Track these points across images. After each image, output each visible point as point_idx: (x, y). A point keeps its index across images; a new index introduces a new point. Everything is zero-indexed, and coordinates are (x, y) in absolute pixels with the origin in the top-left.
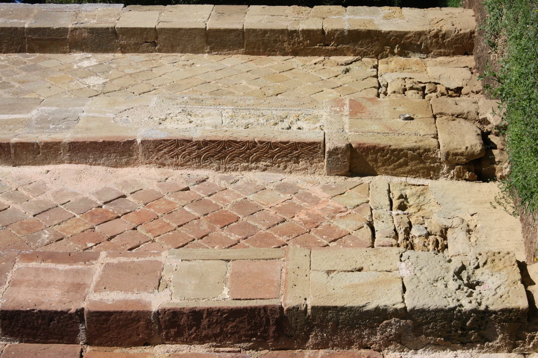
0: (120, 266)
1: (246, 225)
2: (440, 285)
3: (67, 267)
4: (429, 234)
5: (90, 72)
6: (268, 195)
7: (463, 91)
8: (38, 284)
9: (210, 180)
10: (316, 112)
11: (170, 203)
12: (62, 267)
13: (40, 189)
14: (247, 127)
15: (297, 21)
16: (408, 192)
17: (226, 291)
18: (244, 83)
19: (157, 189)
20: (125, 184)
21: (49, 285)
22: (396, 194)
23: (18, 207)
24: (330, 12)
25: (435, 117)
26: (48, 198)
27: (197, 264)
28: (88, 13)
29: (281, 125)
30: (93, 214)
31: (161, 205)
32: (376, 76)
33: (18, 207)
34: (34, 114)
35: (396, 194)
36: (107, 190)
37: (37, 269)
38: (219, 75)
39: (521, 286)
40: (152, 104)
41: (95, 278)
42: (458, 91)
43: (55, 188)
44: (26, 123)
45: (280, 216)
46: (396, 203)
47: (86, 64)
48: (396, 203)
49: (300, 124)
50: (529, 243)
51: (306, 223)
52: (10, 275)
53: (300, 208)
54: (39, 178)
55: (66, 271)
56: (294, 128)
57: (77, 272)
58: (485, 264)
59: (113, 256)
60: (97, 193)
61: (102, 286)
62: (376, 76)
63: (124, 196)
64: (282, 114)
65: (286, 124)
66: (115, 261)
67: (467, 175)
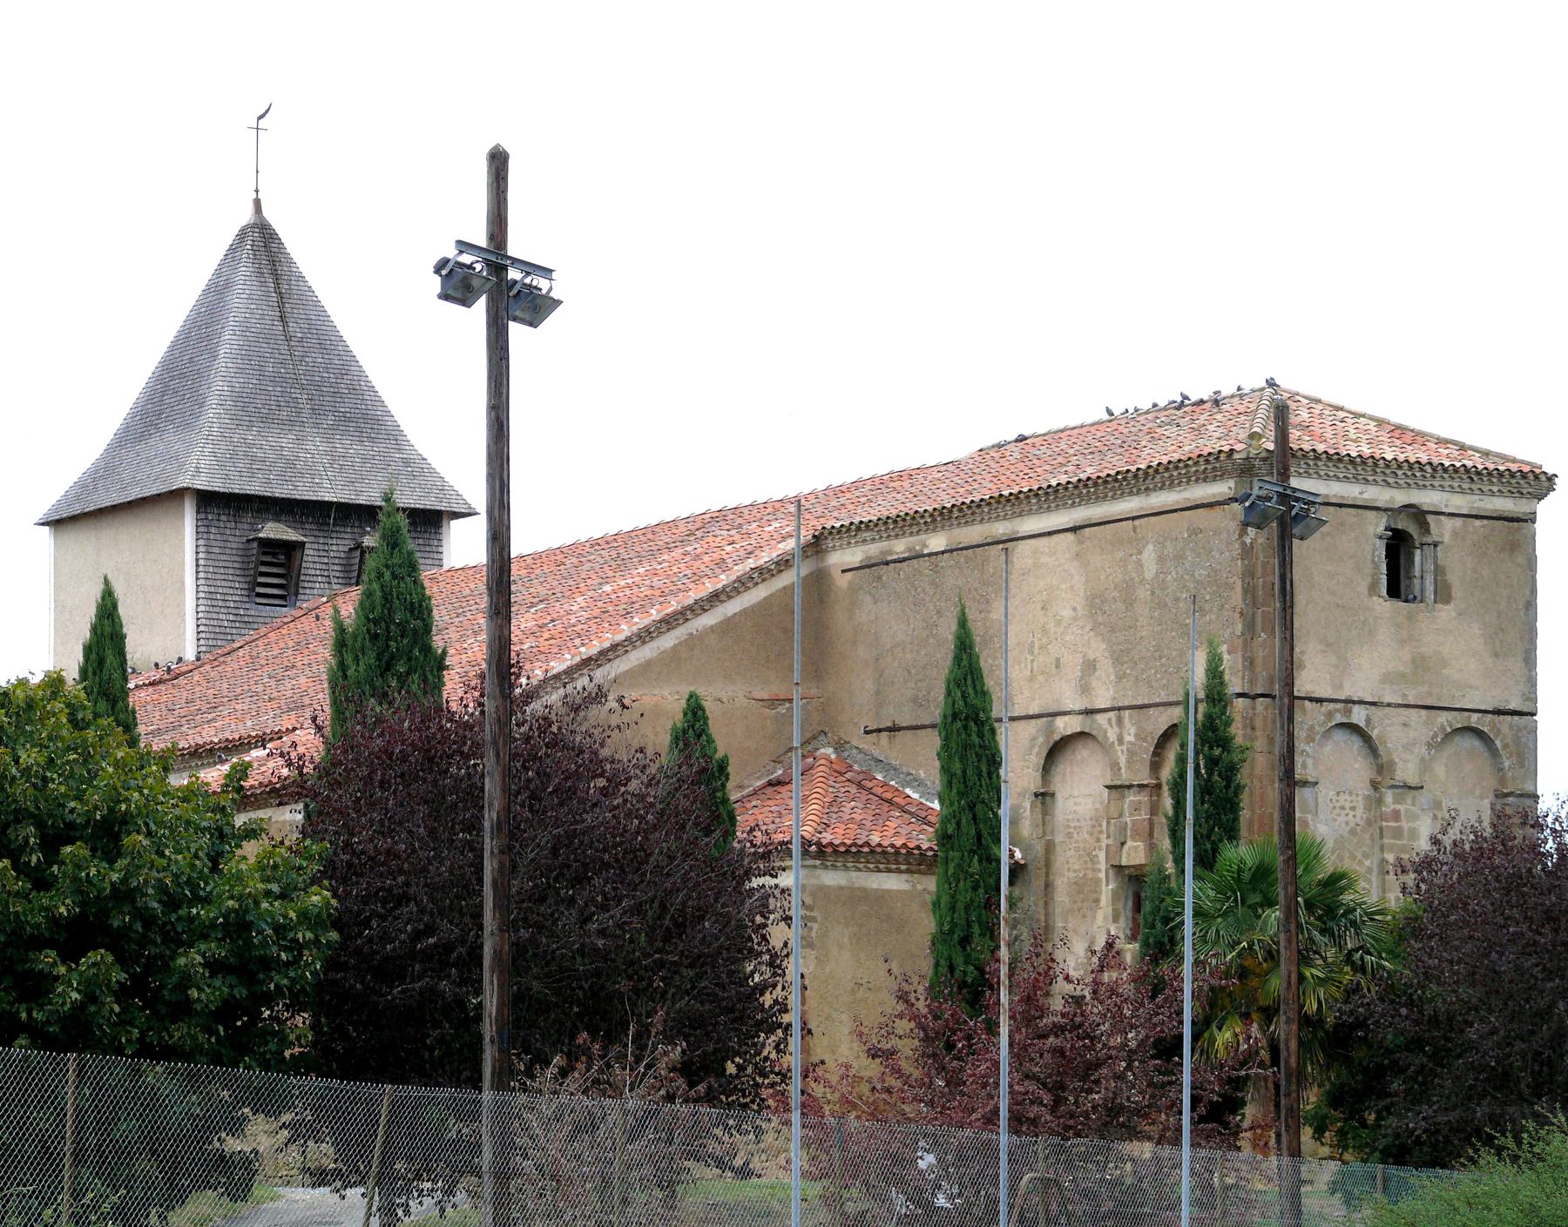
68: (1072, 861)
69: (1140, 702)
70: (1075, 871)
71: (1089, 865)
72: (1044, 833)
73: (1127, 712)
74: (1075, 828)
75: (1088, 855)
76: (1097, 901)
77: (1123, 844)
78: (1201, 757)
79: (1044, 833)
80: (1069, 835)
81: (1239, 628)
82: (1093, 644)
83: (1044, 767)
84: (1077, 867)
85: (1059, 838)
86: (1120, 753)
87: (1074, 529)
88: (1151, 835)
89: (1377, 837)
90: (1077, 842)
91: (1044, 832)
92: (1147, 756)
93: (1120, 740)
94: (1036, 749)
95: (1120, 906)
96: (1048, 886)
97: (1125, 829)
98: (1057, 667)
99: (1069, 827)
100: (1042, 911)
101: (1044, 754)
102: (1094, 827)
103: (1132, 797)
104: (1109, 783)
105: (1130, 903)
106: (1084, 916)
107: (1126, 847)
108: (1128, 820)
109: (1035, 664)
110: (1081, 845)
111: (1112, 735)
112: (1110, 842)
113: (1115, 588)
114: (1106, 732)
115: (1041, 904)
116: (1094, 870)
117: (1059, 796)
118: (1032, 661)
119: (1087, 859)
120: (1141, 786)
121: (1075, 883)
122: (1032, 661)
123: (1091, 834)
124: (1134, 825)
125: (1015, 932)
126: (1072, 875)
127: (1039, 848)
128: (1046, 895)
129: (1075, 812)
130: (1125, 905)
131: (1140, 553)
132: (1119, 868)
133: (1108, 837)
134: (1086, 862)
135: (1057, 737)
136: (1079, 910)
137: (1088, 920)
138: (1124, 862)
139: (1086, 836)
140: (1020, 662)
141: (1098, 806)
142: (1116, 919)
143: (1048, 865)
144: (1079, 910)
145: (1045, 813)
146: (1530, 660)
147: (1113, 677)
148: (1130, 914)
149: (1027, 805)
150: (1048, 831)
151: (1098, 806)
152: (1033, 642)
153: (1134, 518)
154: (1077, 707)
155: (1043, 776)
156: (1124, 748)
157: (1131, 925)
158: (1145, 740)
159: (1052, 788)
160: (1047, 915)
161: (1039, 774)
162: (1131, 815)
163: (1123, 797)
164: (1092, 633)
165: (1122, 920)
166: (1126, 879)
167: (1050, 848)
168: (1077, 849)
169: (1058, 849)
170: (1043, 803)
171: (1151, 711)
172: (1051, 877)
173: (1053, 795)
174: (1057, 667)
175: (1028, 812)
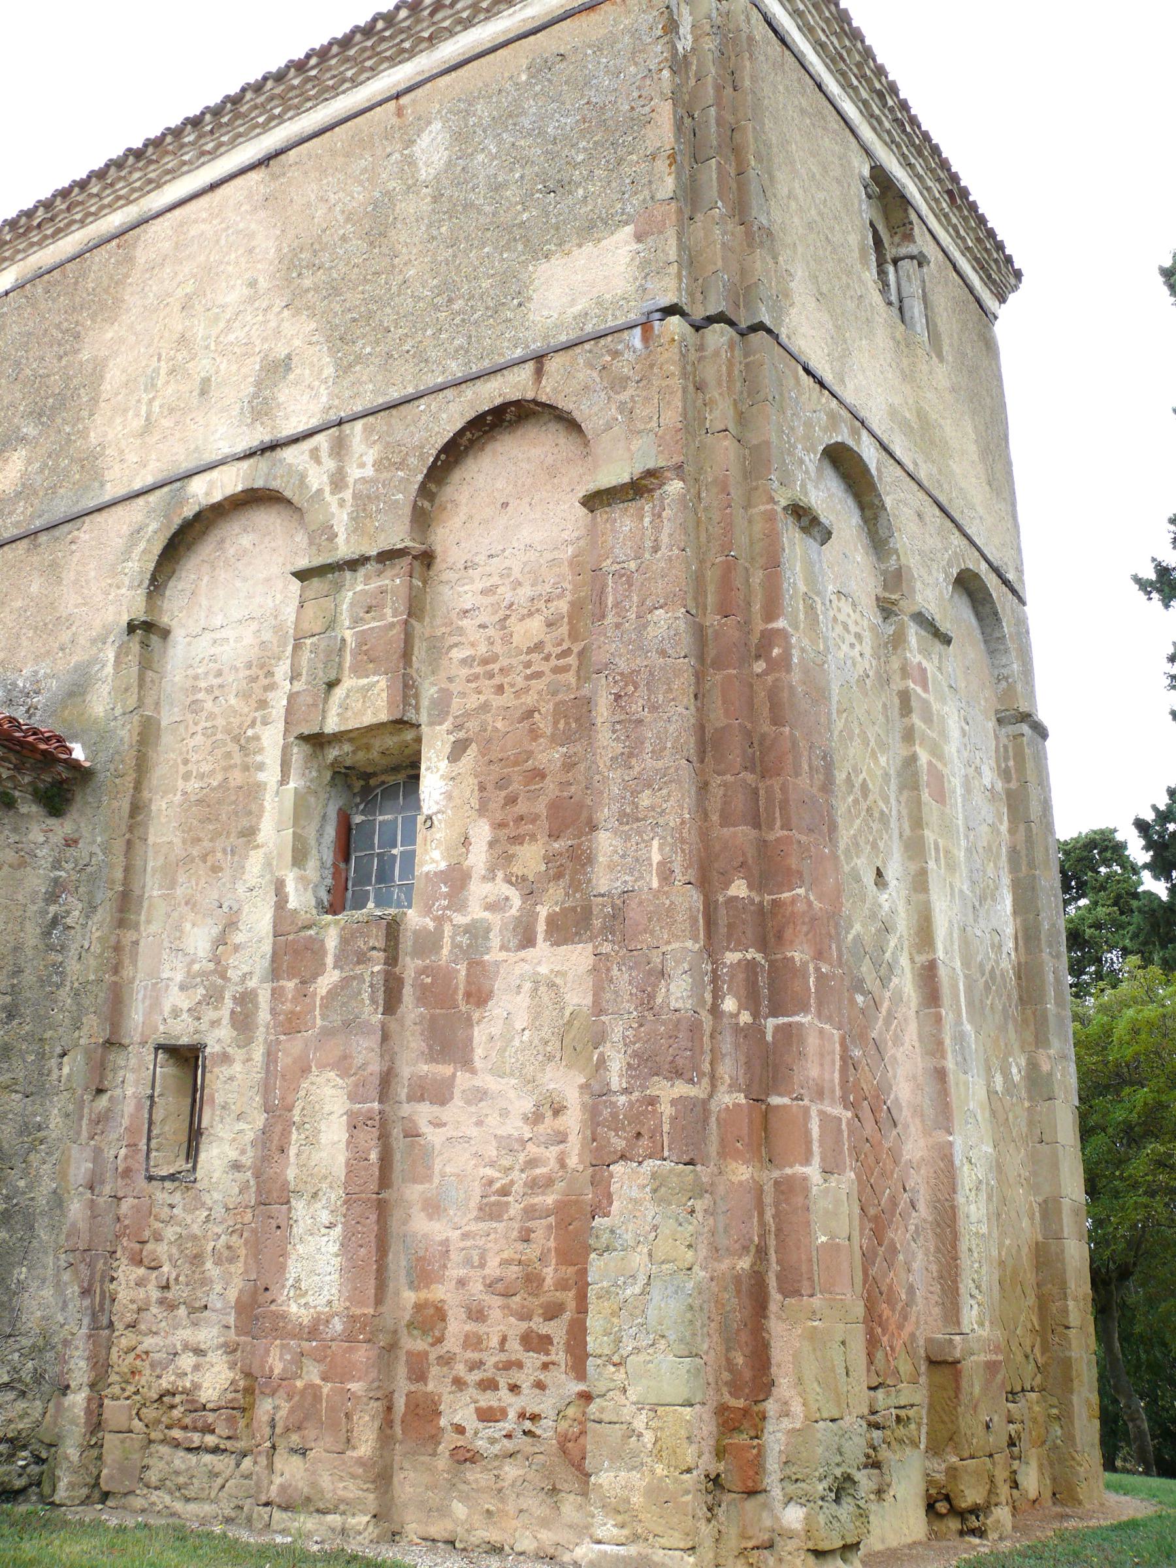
0: (840, 1131)
1: (876, 1254)
2: (838, 1459)
3: (837, 1081)
4: (874, 1449)
5: (1006, 1075)
6: (903, 1275)
7: (1015, 1491)
8: (822, 1055)
9: (914, 1214)
10: (987, 1323)
11: (892, 1173)
12: (837, 1075)
13: (897, 1041)
14: (970, 1250)
15: (1075, 1299)
16: (913, 1426)
17: (824, 1239)
18: (1007, 1242)
19: (903, 1160)
20: (906, 1126)
21: (822, 1065)
22: (911, 1413)
23: (880, 1022)
24: (1088, 1336)
25: (991, 1456)
26: (890, 1051)
27: (845, 1209)
28: (217, 635)
29: (972, 1285)
30: (878, 1097)
31: (889, 1166)
32: (1023, 1390)
33: (880, 1022)
34: (968, 1027)
35: (911, 1413)
36: (900, 1109)
37: (834, 1052)
38: (1013, 1214)
39: (840, 1544)
40: (984, 1148)
41: (829, 1110)
42: (1015, 1485)
43: (899, 1055)
44: (958, 1022)
45: (884, 1288)
46: (902, 1413)
47: (1014, 1070)
48: (902, 1413)
49: (976, 1307)
50: (892, 1555)
51: (880, 1316)
52: (827, 1027)
53: (893, 1310)
54: (907, 1039)
55: (832, 1081)
56: (973, 1302)
57: (833, 1091)
58: (859, 1507)
59: (848, 1124)
60: (897, 1099)
61: (823, 1116)
62: (1023, 1390)
63: (895, 1125)
64: (984, 1288)
65: (975, 1292)
66: (844, 1126)
67: (933, 1491)
68: (194, 757)
69: (395, 394)
70: (201, 776)
71: (237, 758)
72: (140, 704)
73: (359, 425)
74: (209, 690)
75: (235, 738)
76: (249, 833)
77: (331, 685)
78: (347, 748)
79: (140, 704)
80: (195, 707)
81: (668, 185)
82: (288, 328)
83: (153, 579)
84: (205, 768)
85: (167, 717)
86: (334, 508)
87: (264, 162)
88: (407, 655)
89: (895, 712)
90: (211, 716)
91: (140, 699)
92: (404, 498)
93: (338, 481)
94: (143, 545)
95: (311, 832)
96: (137, 809)
97: (341, 650)
98: (203, 393)
99: (195, 689)
100: (119, 860)
101: (157, 549)
102: (254, 679)
103: (358, 586)
104: (303, 563)
105: (331, 832)
106: (216, 869)
107: (339, 692)
108: (348, 634)
109: (156, 404)
110: (220, 722)
111: (317, 478)
112: (298, 686)
113: (348, 220)
114: (303, 477)
115: (119, 846)
116: (246, 768)
117: (179, 636)
118: (151, 401)
119: (233, 747)
120: (387, 557)
121: (199, 802)
122: (151, 401)
123: (245, 695)
124: (360, 645)
125: (53, 909)
126: (194, 785)
127: (126, 733)
128: (131, 829)
129: (213, 658)
130: (320, 832)
131: (411, 143)
132: (317, 741)
133: (294, 677)
134: (228, 755)
135: (189, 511)
136: (204, 857)
137: (226, 876)
138: (332, 725)
139: (233, 701)
140: (125, 411)
141: (267, 636)
142: (299, 858)
143: (142, 766)
144: (204, 857)
145: (146, 664)
146: (1013, 505)
147: (329, 371)
148: (329, 856)
149: (110, 655)
150: (149, 701)
151: (267, 636)
152: (157, 371)
153: (398, 96)
154: (241, 447)
155: (150, 596)
156: (348, 495)
157: (329, 881)
158: (401, 465)
159: (165, 620)
160: (127, 870)
161: (141, 592)
162: (356, 621)
163: (338, 587)
164: (286, 313)
165: (312, 864)
166: (328, 775)
167: (148, 733)
168: (209, 732)
169: (166, 739)
170: (145, 645)
171: (422, 405)
172: (146, 794)
173: (165, 633)
174: (203, 393)
175: (109, 669)
